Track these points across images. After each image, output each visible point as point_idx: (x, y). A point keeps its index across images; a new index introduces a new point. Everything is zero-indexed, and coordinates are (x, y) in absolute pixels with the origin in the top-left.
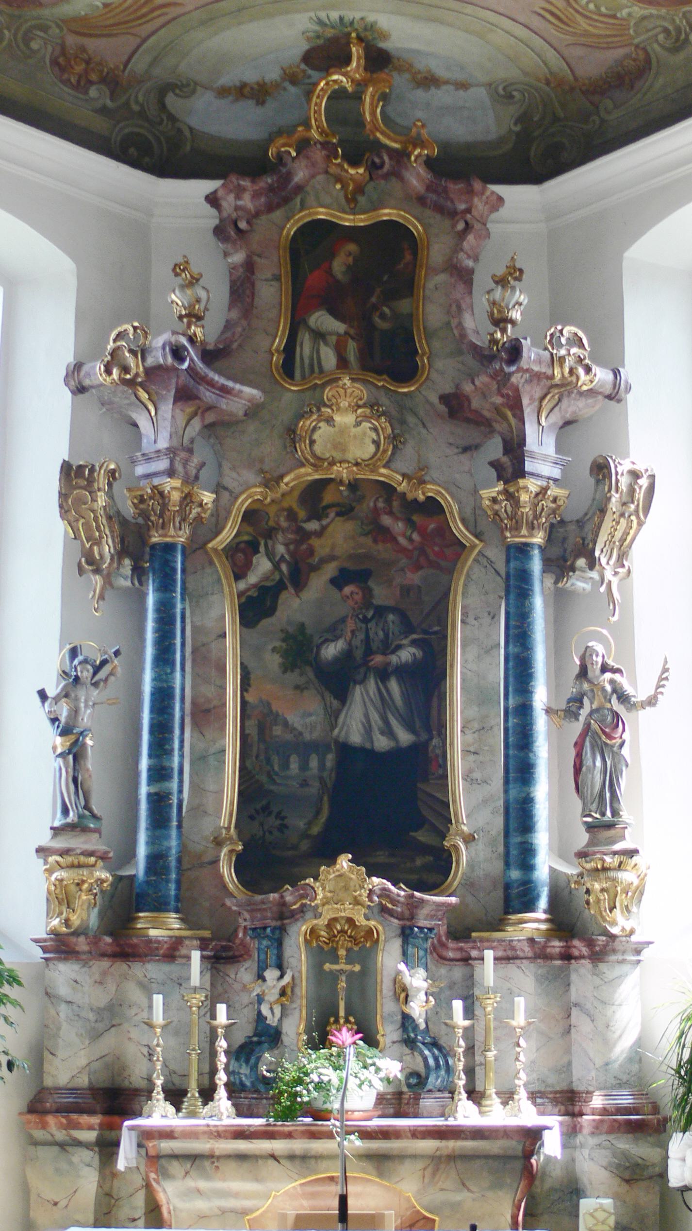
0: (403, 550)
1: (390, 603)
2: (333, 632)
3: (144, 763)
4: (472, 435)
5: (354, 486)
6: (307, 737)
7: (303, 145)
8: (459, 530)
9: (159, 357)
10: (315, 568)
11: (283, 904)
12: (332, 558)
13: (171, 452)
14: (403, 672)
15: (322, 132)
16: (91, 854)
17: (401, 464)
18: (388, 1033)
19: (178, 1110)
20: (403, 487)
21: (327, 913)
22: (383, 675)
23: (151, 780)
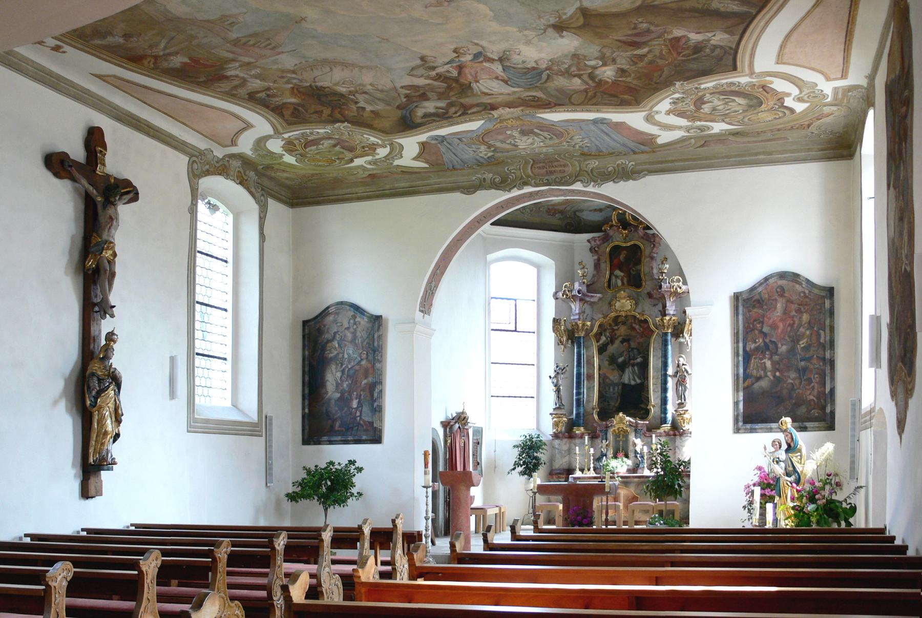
0: (638, 332)
1: (635, 347)
2: (621, 355)
3: (575, 391)
4: (656, 302)
5: (626, 317)
6: (615, 382)
7: (611, 226)
8: (652, 327)
9: (575, 293)
10: (616, 339)
11: (607, 424)
12: (620, 336)
13: (579, 314)
14: (638, 364)
15: (616, 223)
16: (562, 414)
17: (638, 310)
18: (631, 455)
19: (583, 473)
20: (638, 316)
21: (617, 427)
22: (633, 365)
23: (576, 395)
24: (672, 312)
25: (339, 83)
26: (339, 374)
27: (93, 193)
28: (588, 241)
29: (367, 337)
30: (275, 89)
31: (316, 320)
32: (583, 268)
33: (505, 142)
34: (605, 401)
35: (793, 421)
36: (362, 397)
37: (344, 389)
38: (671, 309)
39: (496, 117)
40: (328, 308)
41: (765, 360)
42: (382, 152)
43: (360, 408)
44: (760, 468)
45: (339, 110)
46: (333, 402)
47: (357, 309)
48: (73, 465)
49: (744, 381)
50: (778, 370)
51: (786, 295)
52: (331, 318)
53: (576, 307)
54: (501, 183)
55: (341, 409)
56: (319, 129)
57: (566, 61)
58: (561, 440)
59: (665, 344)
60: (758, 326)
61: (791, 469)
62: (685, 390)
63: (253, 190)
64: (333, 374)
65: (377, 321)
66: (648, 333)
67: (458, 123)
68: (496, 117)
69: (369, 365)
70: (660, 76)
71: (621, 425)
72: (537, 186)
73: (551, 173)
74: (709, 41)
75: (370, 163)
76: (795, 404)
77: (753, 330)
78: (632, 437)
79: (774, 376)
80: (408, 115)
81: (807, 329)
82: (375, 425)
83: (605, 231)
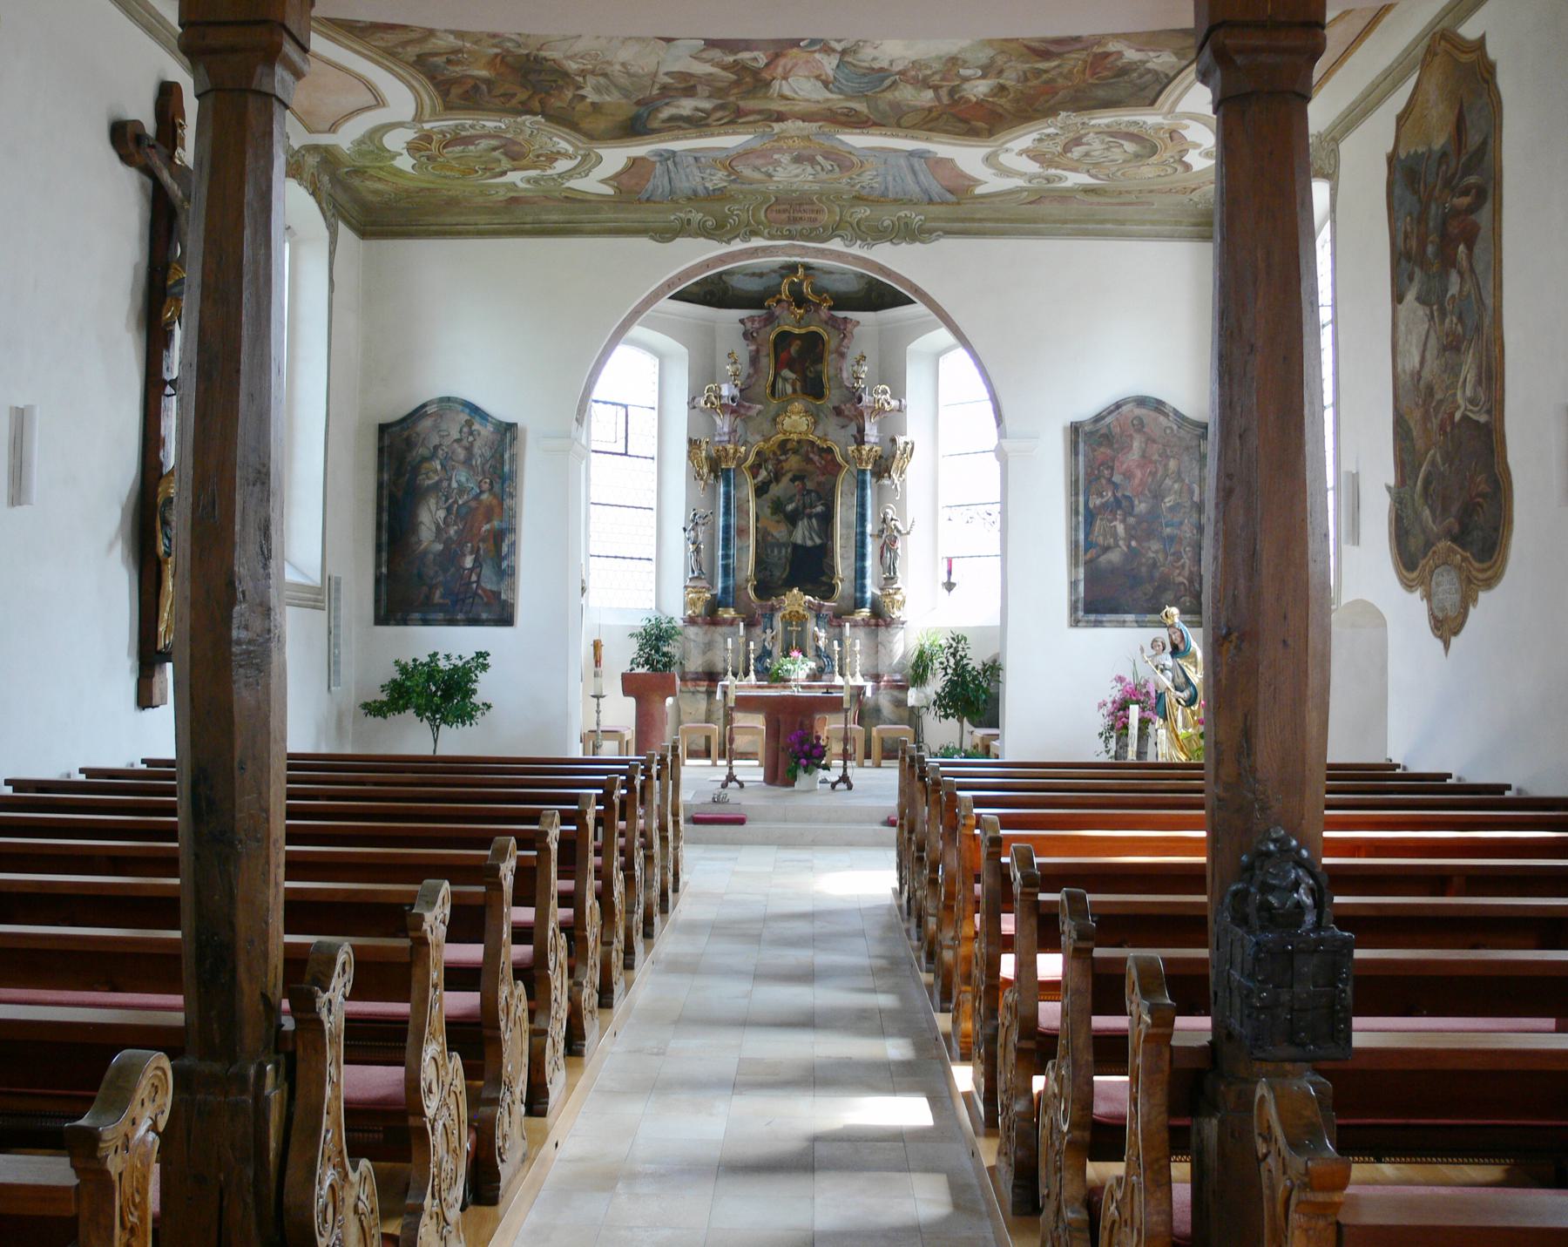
2: (791, 500)
5: (799, 442)
8: (839, 459)
10: (784, 475)
13: (730, 433)
14: (817, 516)
21: (789, 609)
22: (810, 517)
24: (873, 439)
25: (576, 55)
26: (441, 514)
27: (177, 196)
28: (742, 321)
29: (492, 456)
30: (469, 52)
31: (404, 425)
32: (735, 363)
33: (759, 170)
34: (766, 569)
35: (1182, 612)
36: (482, 552)
37: (450, 538)
38: (872, 432)
39: (775, 131)
40: (424, 406)
41: (1116, 523)
42: (562, 165)
43: (478, 570)
44: (1120, 679)
45: (543, 95)
46: (431, 557)
47: (475, 410)
48: (129, 654)
49: (1086, 551)
50: (1132, 537)
51: (1145, 430)
52: (427, 423)
53: (723, 423)
54: (715, 229)
55: (445, 571)
56: (487, 120)
57: (934, 65)
58: (700, 627)
59: (862, 486)
60: (1106, 472)
61: (1182, 680)
62: (895, 558)
63: (324, 205)
64: (431, 512)
65: (508, 430)
66: (832, 468)
67: (712, 135)
68: (775, 131)
69: (495, 502)
70: (1047, 101)
71: (796, 608)
72: (772, 237)
73: (795, 220)
74: (1145, 62)
75: (528, 181)
76: (1159, 587)
77: (1098, 478)
78: (812, 626)
79: (1129, 546)
80: (645, 115)
81: (1175, 482)
82: (503, 597)
83: (769, 308)
